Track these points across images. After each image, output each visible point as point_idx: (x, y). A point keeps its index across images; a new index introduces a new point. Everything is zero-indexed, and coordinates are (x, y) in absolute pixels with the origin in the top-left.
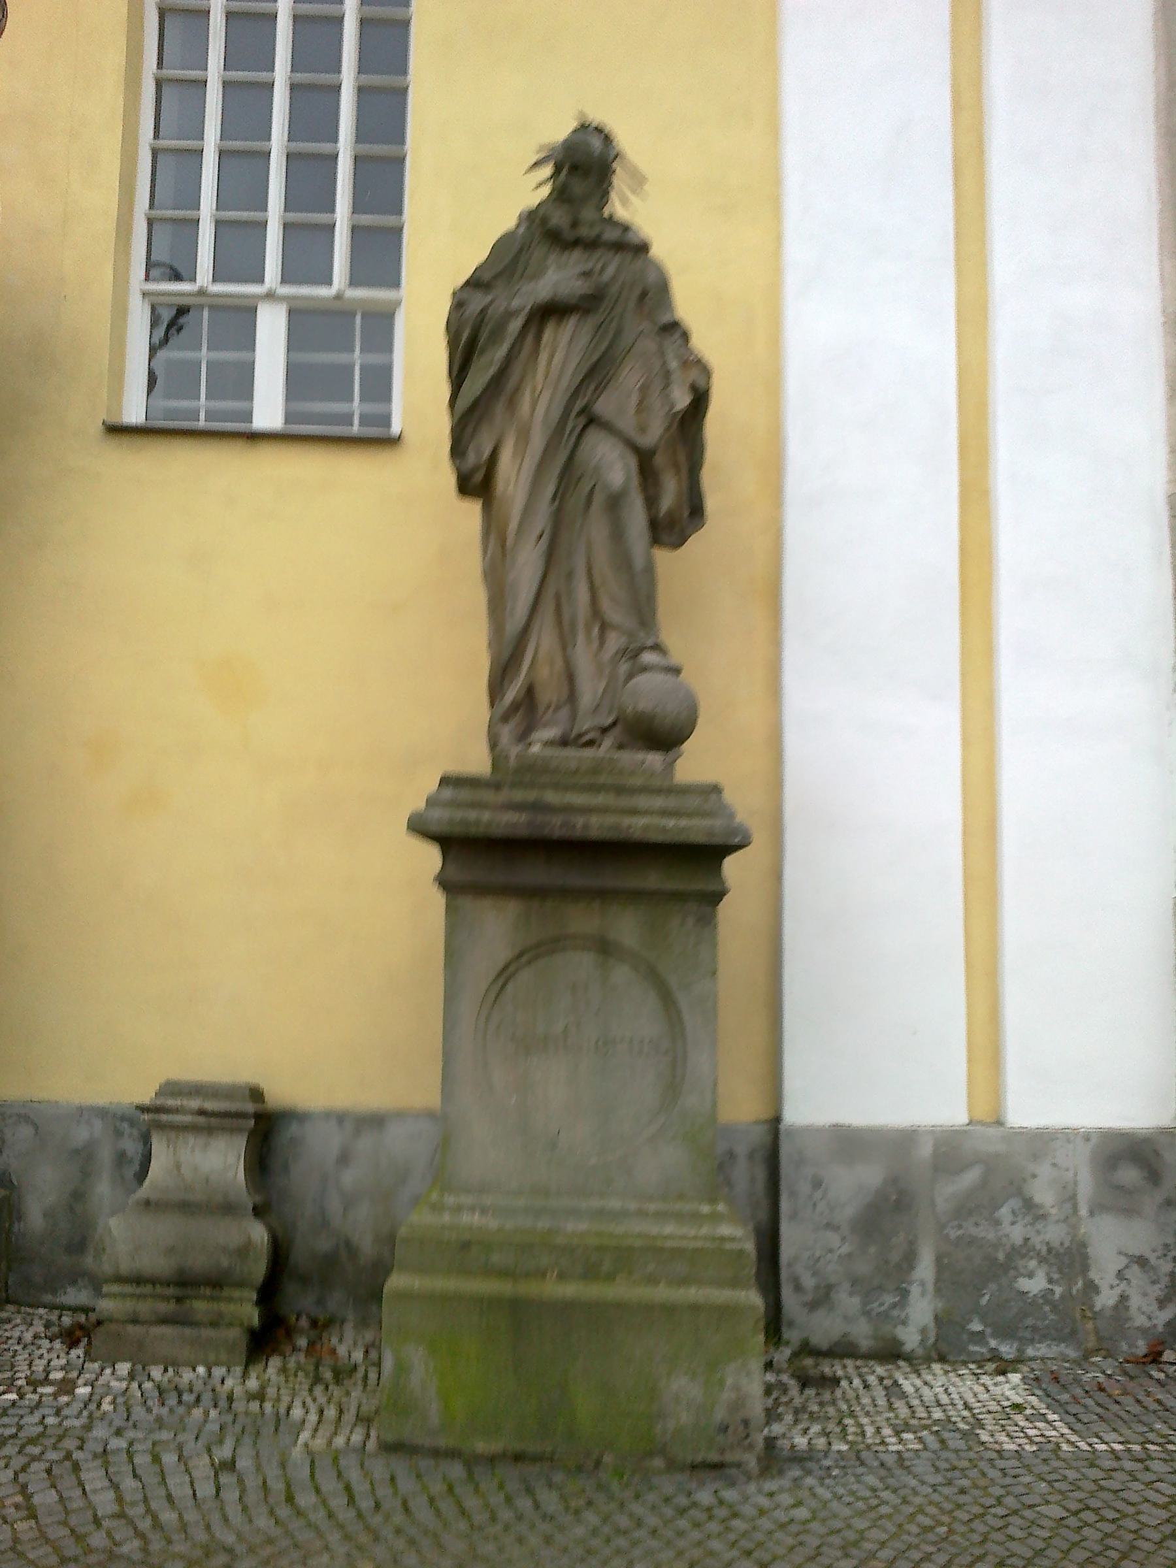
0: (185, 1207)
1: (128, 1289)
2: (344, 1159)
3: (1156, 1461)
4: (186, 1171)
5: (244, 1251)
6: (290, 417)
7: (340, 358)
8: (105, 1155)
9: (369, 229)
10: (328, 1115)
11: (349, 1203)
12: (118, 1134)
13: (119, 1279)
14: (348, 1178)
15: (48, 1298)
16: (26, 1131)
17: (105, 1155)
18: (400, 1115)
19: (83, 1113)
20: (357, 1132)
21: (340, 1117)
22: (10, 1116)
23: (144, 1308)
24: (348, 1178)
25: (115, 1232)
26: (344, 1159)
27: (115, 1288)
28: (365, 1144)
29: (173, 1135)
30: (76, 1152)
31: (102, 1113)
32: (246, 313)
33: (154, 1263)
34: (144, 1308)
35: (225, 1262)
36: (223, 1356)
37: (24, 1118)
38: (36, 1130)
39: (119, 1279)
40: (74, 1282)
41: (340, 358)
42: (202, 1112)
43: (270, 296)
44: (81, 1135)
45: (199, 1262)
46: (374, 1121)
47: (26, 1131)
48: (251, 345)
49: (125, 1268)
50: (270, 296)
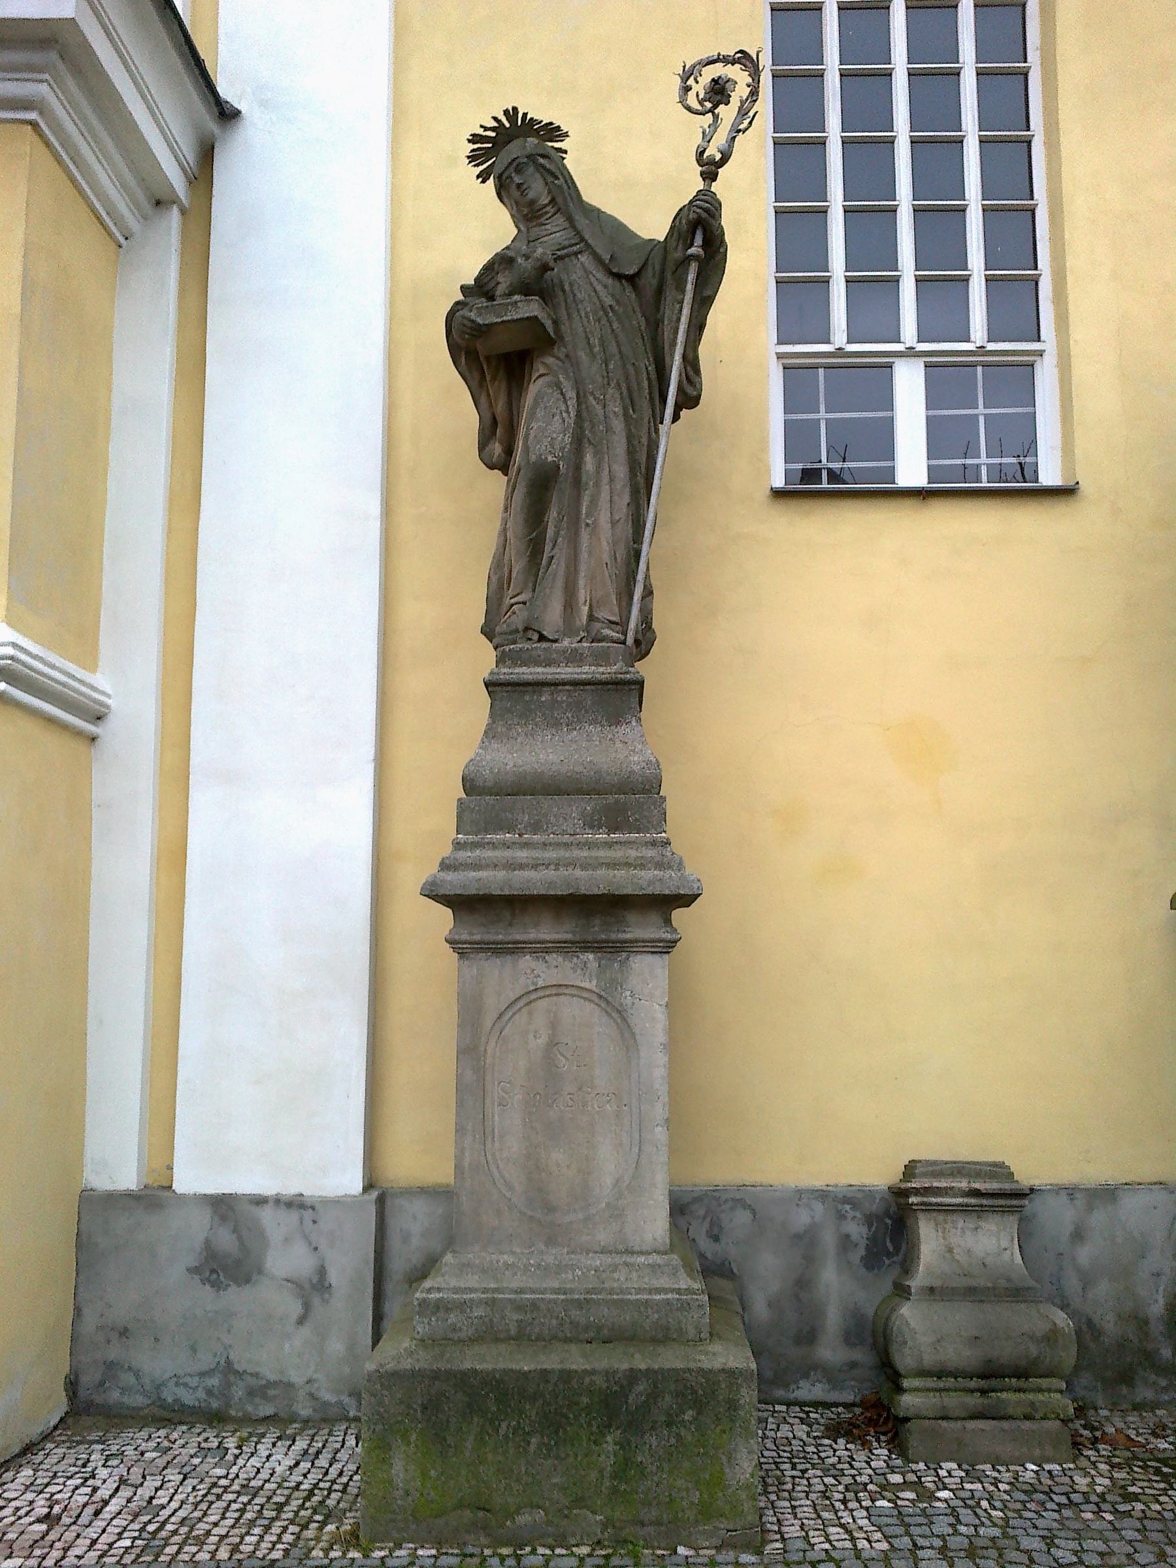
0: (972, 1293)
1: (930, 1383)
2: (1078, 1235)
3: (1033, 1509)
4: (959, 1255)
5: (1052, 1336)
6: (933, 473)
7: (822, 408)
8: (829, 1239)
9: (1002, 278)
10: (1058, 1189)
11: (1087, 1282)
12: (841, 1217)
13: (923, 1373)
14: (1085, 1255)
15: (780, 1393)
16: (742, 1217)
17: (829, 1239)
18: (1129, 1186)
19: (801, 1195)
20: (1090, 1208)
21: (1071, 1191)
22: (726, 1201)
23: (952, 1401)
24: (1085, 1255)
25: (913, 1324)
26: (1078, 1235)
27: (916, 1383)
28: (1098, 1218)
29: (941, 1217)
30: (798, 1237)
31: (822, 1195)
32: (883, 368)
33: (957, 1354)
34: (952, 1401)
35: (1034, 1350)
36: (1049, 1451)
37: (740, 1203)
38: (754, 1213)
39: (923, 1373)
40: (806, 1376)
41: (822, 408)
42: (976, 1193)
43: (910, 353)
44: (802, 1219)
45: (1006, 1352)
46: (1106, 1194)
47: (742, 1217)
48: (1031, 400)
49: (929, 1360)
50: (910, 353)
